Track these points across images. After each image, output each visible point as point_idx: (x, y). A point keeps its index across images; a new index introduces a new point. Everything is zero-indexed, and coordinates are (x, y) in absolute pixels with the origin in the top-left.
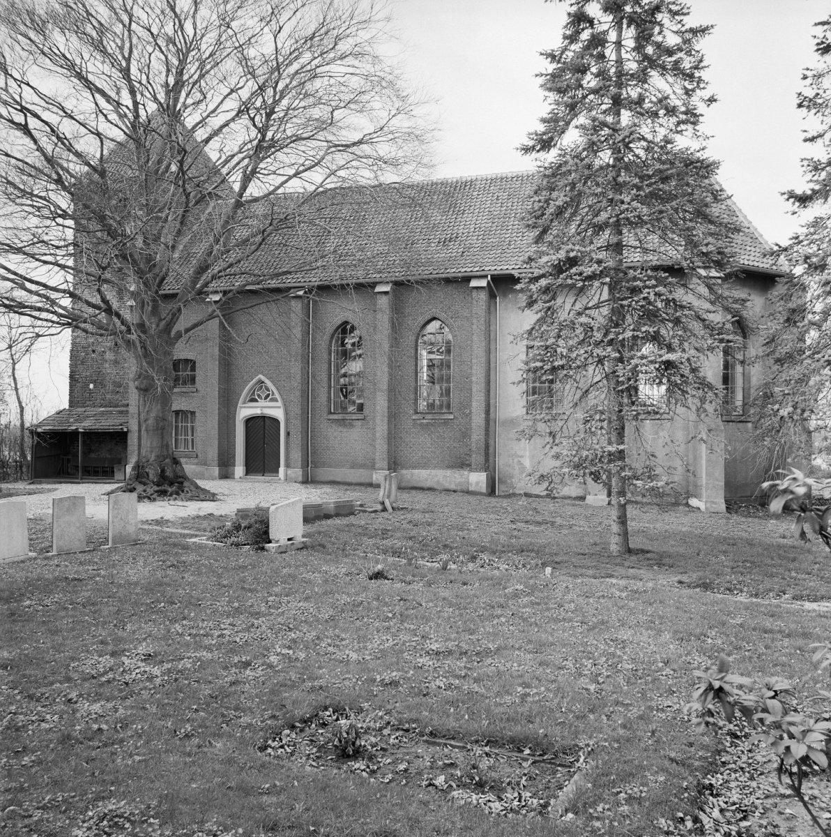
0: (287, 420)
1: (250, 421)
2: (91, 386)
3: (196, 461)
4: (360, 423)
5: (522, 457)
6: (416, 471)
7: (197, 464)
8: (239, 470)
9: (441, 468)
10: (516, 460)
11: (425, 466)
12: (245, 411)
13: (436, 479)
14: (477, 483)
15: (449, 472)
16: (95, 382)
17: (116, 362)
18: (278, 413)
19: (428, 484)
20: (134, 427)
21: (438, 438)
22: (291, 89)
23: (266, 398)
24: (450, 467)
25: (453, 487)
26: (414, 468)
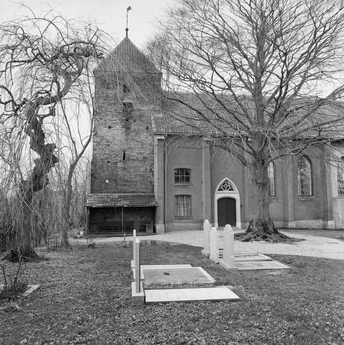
0: (242, 198)
1: (220, 200)
2: (107, 181)
3: (192, 221)
4: (275, 201)
5: (338, 213)
6: (300, 221)
7: (193, 223)
8: (216, 224)
9: (310, 219)
10: (336, 215)
11: (303, 219)
12: (219, 195)
13: (309, 224)
14: (331, 225)
15: (314, 221)
16: (109, 179)
17: (124, 169)
18: (235, 195)
19: (306, 227)
20: (161, 203)
21: (308, 206)
22: (248, 77)
23: (227, 189)
24: (314, 219)
25: (316, 227)
26: (300, 220)
